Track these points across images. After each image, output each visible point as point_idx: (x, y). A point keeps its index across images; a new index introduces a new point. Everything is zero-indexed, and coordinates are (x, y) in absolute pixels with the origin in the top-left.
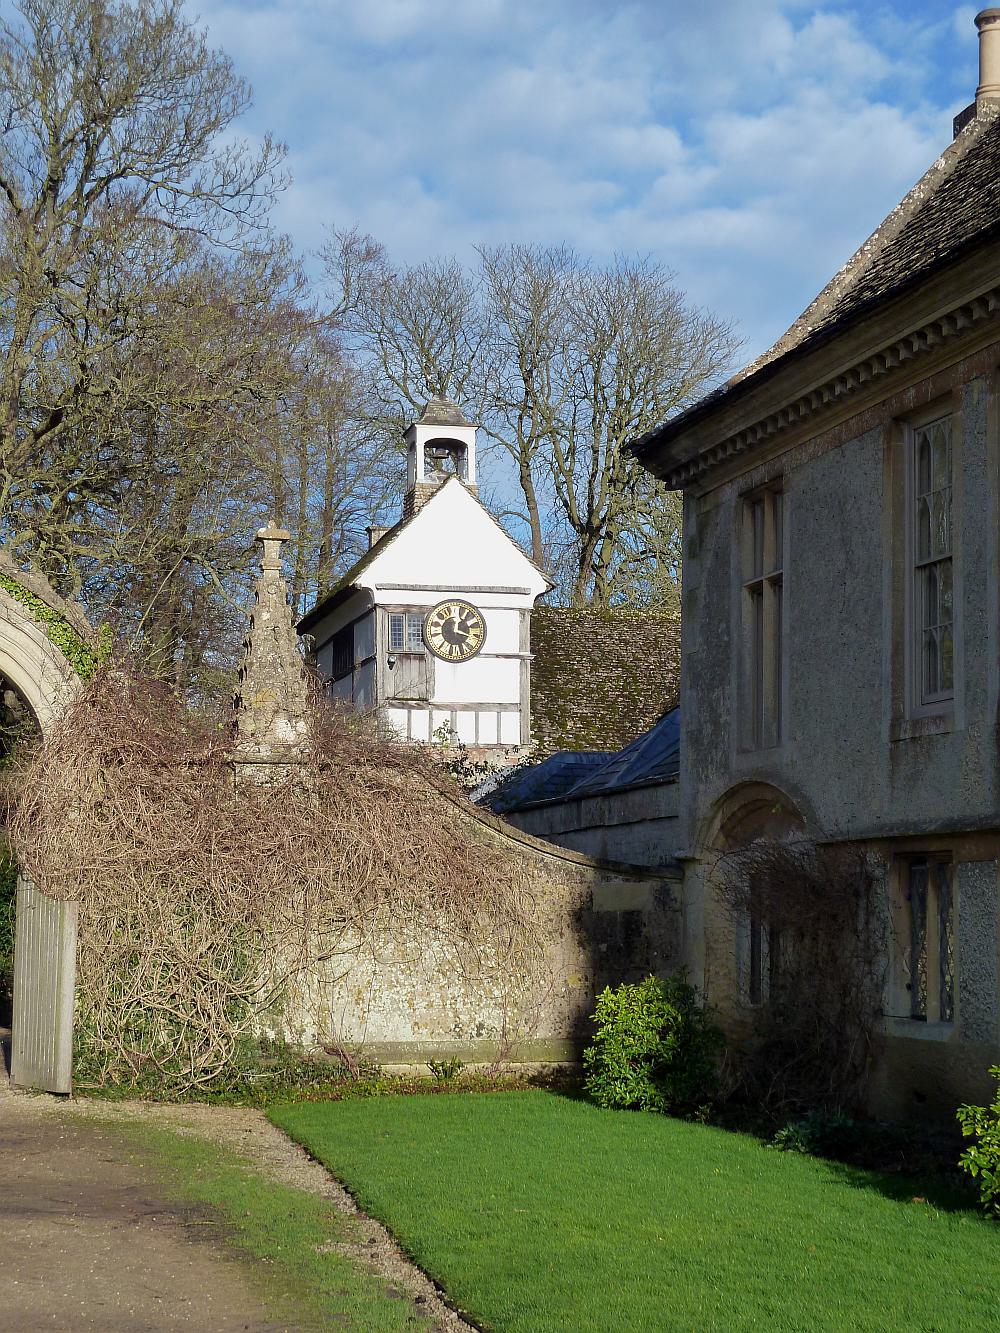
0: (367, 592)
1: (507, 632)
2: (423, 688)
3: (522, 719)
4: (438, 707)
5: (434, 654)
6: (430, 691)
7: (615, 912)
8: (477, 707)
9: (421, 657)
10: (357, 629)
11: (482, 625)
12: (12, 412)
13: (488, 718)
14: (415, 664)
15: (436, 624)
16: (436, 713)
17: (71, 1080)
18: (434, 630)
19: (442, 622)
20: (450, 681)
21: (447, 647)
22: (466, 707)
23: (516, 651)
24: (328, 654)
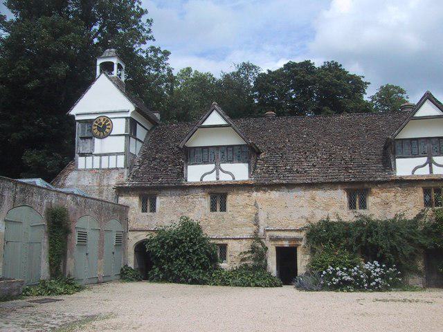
6: (93, 150)
15: (95, 126)
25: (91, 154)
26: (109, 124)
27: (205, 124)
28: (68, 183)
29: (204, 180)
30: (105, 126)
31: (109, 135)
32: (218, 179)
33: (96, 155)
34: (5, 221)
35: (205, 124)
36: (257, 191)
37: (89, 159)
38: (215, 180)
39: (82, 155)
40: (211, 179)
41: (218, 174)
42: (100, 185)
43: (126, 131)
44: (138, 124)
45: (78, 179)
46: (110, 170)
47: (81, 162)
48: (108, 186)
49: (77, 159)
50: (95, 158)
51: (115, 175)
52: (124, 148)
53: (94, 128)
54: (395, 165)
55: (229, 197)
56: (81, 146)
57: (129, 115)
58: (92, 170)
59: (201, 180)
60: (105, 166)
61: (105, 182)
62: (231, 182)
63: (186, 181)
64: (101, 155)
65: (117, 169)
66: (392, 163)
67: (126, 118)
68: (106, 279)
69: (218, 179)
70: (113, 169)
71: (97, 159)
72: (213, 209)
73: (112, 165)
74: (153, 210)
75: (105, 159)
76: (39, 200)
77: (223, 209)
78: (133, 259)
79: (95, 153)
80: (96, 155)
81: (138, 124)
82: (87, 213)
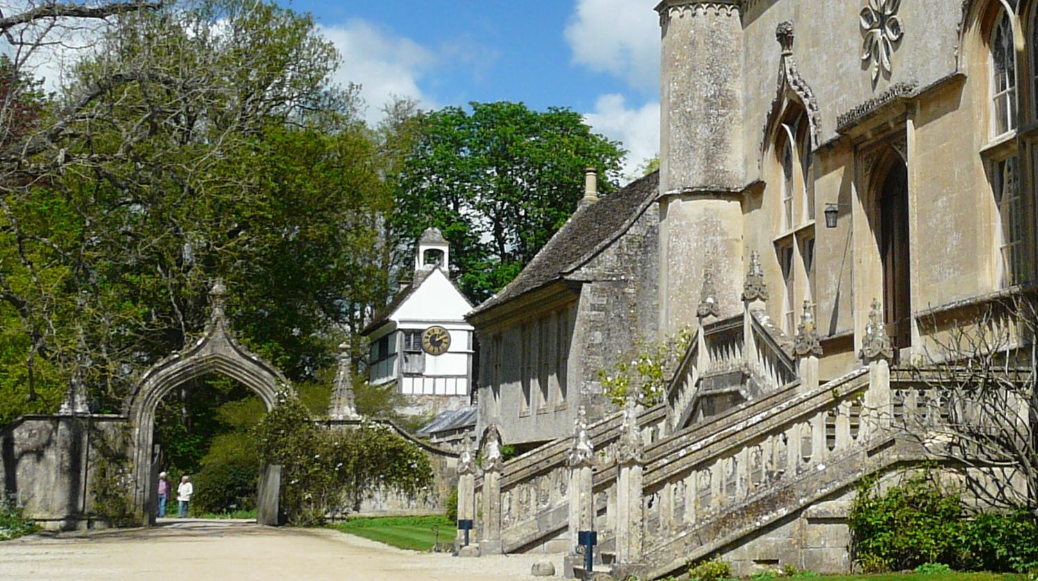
0: (395, 323)
1: (461, 340)
2: (421, 367)
3: (468, 382)
4: (427, 377)
5: (425, 352)
6: (424, 369)
7: (938, 331)
8: (446, 377)
9: (420, 353)
10: (390, 337)
11: (449, 337)
12: (230, 431)
13: (451, 381)
14: (417, 356)
15: (427, 338)
16: (426, 379)
17: (482, 557)
18: (426, 340)
19: (428, 340)
20: (433, 364)
21: (432, 348)
22: (441, 377)
23: (466, 350)
24: (377, 347)
25: (419, 375)
31: (446, 351)
37: (418, 380)
60: (440, 391)
64: (434, 377)
73: (451, 391)
75: (440, 382)
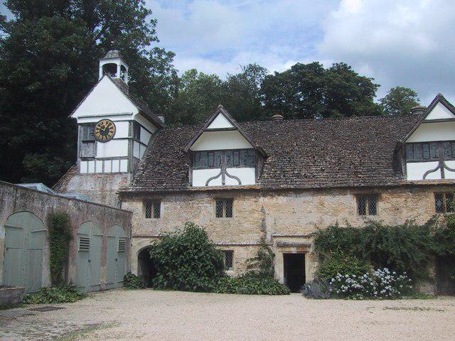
6: (96, 154)
15: (98, 129)
25: (93, 158)
26: (112, 128)
27: (210, 127)
28: (70, 188)
29: (209, 185)
30: (107, 130)
31: (112, 138)
32: (224, 184)
33: (99, 159)
34: (5, 227)
35: (210, 127)
36: (264, 196)
37: (91, 163)
38: (221, 184)
39: (85, 159)
40: (217, 183)
41: (223, 179)
42: (102, 190)
43: (130, 135)
44: (141, 128)
45: (81, 184)
46: (113, 174)
47: (83, 166)
48: (111, 191)
49: (79, 164)
50: (98, 162)
51: (119, 180)
52: (127, 152)
53: (97, 131)
54: (406, 169)
55: (235, 202)
56: (83, 150)
57: (132, 118)
58: (94, 174)
59: (207, 185)
60: (107, 170)
61: (108, 187)
62: (237, 186)
63: (191, 186)
64: (103, 159)
65: (120, 173)
66: (403, 167)
67: (130, 121)
68: (109, 287)
69: (224, 184)
70: (116, 173)
71: (99, 163)
72: (219, 215)
73: (116, 170)
74: (157, 215)
75: (108, 163)
76: (40, 206)
77: (229, 214)
78: (137, 266)
79: (97, 157)
80: (99, 159)
81: (141, 128)
82: (90, 219)
